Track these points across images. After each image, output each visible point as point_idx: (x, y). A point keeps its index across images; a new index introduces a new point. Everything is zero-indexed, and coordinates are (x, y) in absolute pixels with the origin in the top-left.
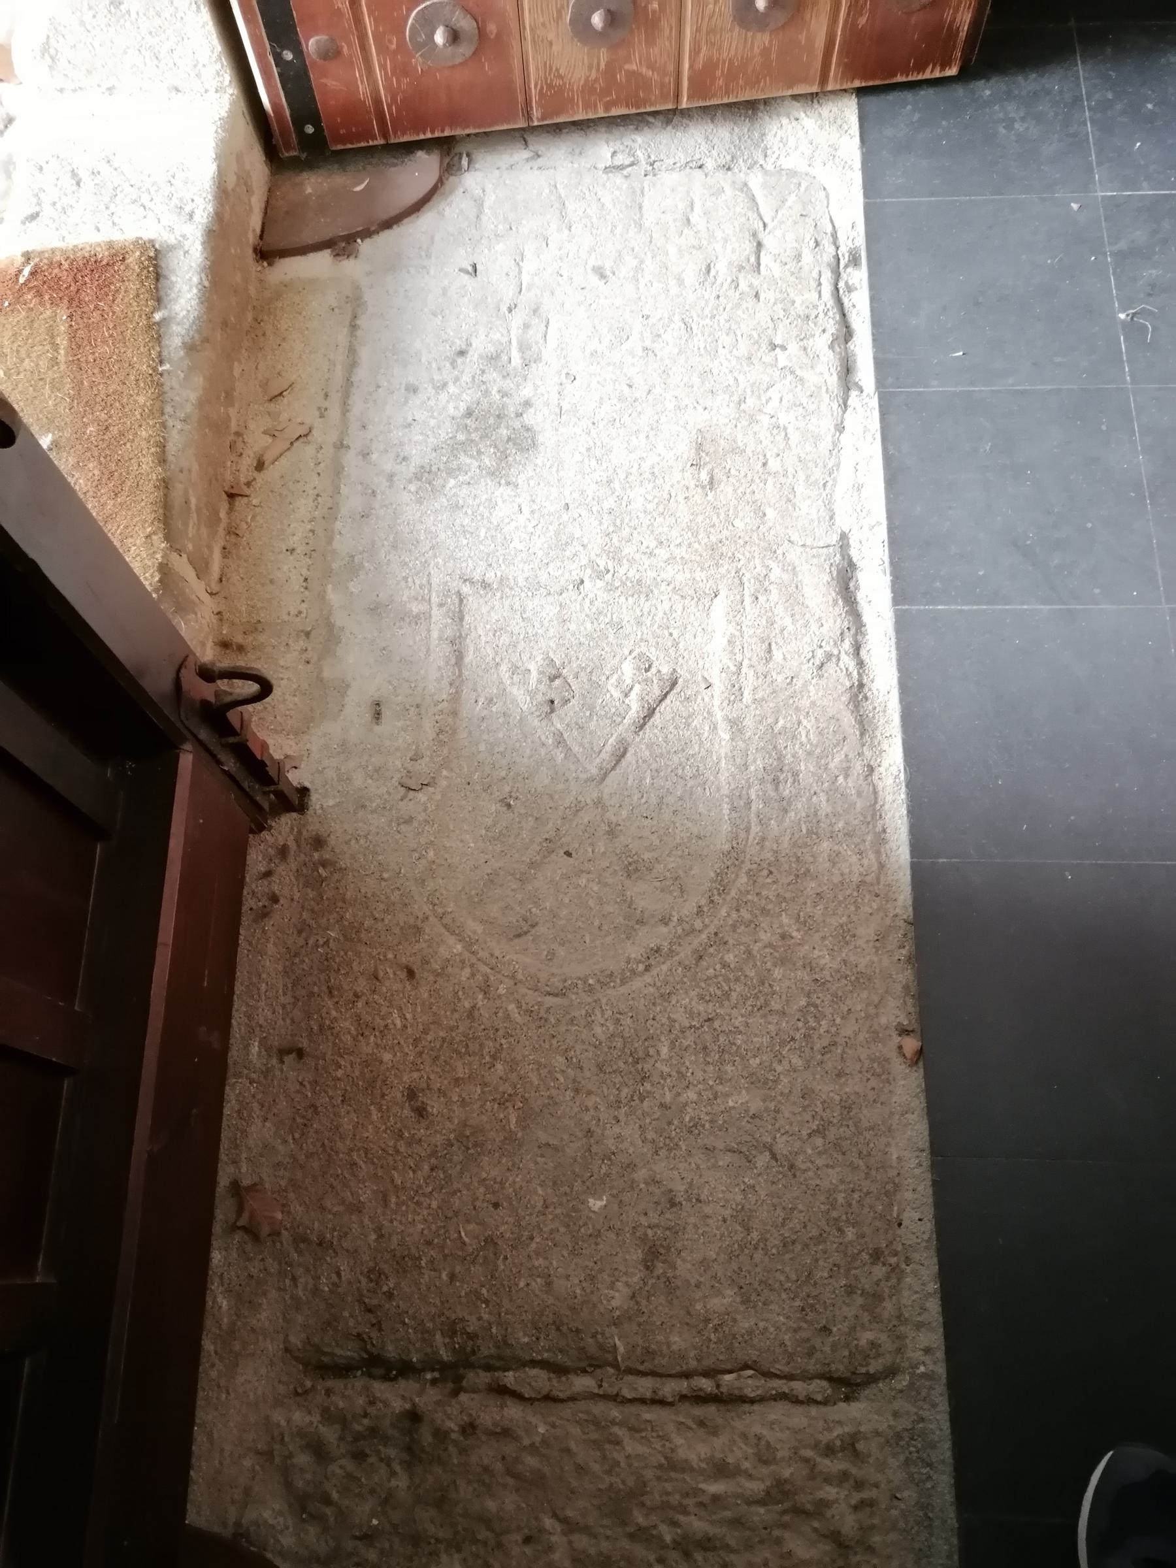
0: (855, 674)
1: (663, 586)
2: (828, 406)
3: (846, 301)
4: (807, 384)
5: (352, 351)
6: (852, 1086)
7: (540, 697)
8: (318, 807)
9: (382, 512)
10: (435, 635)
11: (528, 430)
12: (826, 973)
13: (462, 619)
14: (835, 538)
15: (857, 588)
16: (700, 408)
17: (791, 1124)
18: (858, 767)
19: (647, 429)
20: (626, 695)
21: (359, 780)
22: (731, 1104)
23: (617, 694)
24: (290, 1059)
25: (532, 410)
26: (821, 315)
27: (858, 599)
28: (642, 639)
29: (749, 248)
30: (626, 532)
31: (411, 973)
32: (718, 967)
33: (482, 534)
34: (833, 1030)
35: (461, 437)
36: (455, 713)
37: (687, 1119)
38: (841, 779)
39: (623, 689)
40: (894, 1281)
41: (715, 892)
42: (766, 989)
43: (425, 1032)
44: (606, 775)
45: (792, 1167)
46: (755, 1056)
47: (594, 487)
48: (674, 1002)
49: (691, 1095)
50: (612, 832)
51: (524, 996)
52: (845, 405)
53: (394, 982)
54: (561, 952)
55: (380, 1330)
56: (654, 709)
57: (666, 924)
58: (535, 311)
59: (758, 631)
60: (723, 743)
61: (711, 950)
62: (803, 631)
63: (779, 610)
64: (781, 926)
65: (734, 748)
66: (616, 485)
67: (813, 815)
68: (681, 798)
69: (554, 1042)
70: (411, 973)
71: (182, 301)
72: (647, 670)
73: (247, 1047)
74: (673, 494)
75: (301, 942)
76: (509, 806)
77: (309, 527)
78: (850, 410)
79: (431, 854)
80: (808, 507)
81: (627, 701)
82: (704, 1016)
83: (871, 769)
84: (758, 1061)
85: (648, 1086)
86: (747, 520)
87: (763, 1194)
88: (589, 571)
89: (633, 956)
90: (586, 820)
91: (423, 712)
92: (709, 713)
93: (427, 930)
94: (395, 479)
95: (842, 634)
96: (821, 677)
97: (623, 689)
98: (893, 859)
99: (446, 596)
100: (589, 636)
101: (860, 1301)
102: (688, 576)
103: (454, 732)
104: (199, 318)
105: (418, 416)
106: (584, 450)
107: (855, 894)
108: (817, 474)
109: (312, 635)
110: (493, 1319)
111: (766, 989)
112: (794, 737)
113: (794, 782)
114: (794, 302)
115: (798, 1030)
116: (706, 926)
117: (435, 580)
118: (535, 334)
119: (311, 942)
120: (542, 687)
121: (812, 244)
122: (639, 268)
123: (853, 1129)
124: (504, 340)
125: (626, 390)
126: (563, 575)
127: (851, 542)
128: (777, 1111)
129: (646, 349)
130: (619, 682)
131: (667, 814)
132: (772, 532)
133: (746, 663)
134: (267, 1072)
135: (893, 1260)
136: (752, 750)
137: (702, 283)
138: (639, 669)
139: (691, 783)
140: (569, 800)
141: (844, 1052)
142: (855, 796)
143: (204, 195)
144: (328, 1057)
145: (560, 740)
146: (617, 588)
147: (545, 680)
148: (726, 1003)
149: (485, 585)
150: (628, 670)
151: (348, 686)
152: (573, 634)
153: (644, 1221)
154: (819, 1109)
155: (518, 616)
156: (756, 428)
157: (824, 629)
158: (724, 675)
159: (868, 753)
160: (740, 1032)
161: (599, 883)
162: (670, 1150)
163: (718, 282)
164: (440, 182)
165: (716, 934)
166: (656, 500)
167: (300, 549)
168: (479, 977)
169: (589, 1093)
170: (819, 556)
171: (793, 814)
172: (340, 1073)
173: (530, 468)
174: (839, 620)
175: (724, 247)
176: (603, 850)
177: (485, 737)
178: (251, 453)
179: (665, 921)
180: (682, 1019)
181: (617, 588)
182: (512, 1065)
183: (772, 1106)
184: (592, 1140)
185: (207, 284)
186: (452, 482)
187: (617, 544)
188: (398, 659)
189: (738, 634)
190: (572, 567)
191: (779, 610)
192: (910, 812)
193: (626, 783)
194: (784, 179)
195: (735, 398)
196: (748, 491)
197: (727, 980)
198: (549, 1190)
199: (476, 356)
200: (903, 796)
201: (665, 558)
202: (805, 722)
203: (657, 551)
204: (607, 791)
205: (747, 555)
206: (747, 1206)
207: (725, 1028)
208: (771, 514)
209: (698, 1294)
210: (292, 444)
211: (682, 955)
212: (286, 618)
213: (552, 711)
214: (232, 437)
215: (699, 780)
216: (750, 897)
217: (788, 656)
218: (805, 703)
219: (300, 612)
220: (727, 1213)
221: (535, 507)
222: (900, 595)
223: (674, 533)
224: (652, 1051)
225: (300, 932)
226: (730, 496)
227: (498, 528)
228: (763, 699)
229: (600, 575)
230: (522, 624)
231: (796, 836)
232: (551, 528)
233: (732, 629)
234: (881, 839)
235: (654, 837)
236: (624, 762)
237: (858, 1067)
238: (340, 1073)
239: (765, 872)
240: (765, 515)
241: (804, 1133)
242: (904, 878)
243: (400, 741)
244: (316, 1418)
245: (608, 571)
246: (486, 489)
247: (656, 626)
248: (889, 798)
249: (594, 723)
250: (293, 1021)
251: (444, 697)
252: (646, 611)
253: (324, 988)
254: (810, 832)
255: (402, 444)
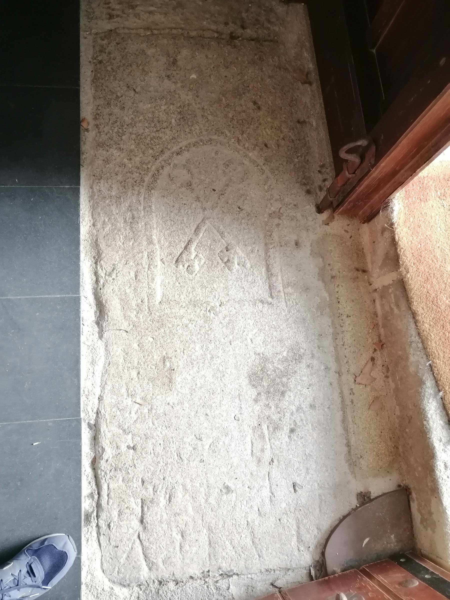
0: (98, 268)
1: (184, 305)
2: (106, 412)
3: (94, 487)
4: (117, 424)
5: (346, 429)
6: (106, 111)
7: (233, 251)
8: (312, 206)
9: (313, 337)
10: (280, 278)
11: (253, 385)
12: (114, 147)
13: (270, 286)
14: (105, 335)
15: (96, 312)
16: (171, 404)
17: (128, 100)
18: (99, 225)
19: (197, 389)
20: (197, 255)
21: (299, 216)
22: (149, 105)
23: (200, 255)
24: (302, 120)
25: (254, 397)
26: (108, 472)
27: (95, 307)
28: (192, 280)
29: (148, 519)
30: (203, 330)
31: (266, 145)
32: (155, 148)
33: (267, 327)
34: (113, 128)
35: (284, 380)
36: (266, 244)
37: (164, 101)
38: (106, 220)
39: (198, 258)
40: (95, 56)
41: (157, 174)
42: (137, 141)
43: (257, 127)
44: (203, 220)
45: (128, 87)
46: (141, 120)
47: (220, 355)
48: (171, 137)
49: (163, 108)
50: (198, 199)
51: (225, 138)
52: (98, 413)
53: (272, 144)
54: (213, 154)
55: (257, 47)
56: (184, 249)
57: (174, 164)
58: (259, 461)
59: (141, 285)
60: (155, 235)
61: (157, 154)
62: (121, 286)
63: (132, 296)
64: (131, 163)
65: (150, 232)
66: (209, 356)
67: (118, 204)
68: (172, 212)
69: (212, 124)
70: (266, 145)
71: (433, 408)
72: (189, 266)
73: (317, 124)
74: (182, 353)
75: (307, 158)
76: (239, 208)
77: (343, 329)
78: (95, 410)
79: (266, 188)
80: (117, 351)
81: (196, 252)
82: (160, 132)
83: (94, 225)
84: (140, 118)
85: (179, 110)
86: (147, 341)
87: (138, 79)
88: (218, 310)
89: (186, 152)
90: (208, 203)
91: (279, 244)
92: (161, 248)
93: (263, 160)
94: (311, 355)
95: (104, 286)
96: (114, 265)
97: (198, 258)
98: (87, 190)
99: (278, 296)
100: (214, 281)
101: (107, 51)
102: (173, 311)
103: (265, 237)
104: (422, 400)
105: (306, 390)
106: (226, 374)
107: (102, 175)
108: (112, 370)
109: (330, 277)
110: (223, 48)
111: (137, 141)
112: (126, 237)
113: (126, 219)
114: (123, 480)
115: (126, 128)
116: (160, 162)
117: (284, 304)
118: (258, 446)
119: (303, 158)
120: (232, 256)
121: (112, 525)
122: (208, 495)
123: (107, 98)
124: (272, 441)
125: (208, 412)
126: (229, 309)
127: (97, 335)
128: (133, 103)
129: (200, 439)
130: (200, 260)
131: (177, 205)
132: (135, 336)
133: (146, 270)
134: (308, 117)
135: (95, 61)
136: (143, 231)
137: (173, 488)
138: (192, 266)
139: (168, 218)
140: (216, 211)
141: (109, 122)
142: (101, 213)
143: (443, 481)
144: (289, 121)
145: (222, 234)
146: (204, 303)
147: (231, 259)
148: (152, 137)
149: (262, 302)
150: (197, 267)
151: (311, 254)
152: (221, 282)
153: (178, 72)
154: (118, 104)
155: (246, 289)
156: (143, 394)
157: (112, 287)
158: (156, 264)
159: (95, 231)
160: (146, 127)
161: (201, 180)
162: (170, 91)
163: (164, 490)
164: (323, 554)
165: (156, 159)
166: (190, 349)
167: (344, 317)
168: (242, 144)
169: (199, 109)
170: (113, 325)
171: (126, 205)
172: (284, 116)
173: (250, 364)
174: (105, 293)
175: (162, 516)
176: (201, 192)
177: (252, 236)
178: (379, 367)
179: (175, 166)
180: (168, 131)
181: (204, 303)
182: (226, 116)
183: (135, 105)
184: (196, 94)
185: (425, 423)
186: (285, 354)
187: (206, 324)
188: (293, 267)
189: (150, 283)
190: (225, 312)
191: (132, 296)
192: (79, 205)
193: (194, 218)
194: (128, 576)
195: (154, 411)
196: (146, 357)
197: (152, 144)
198: (209, 80)
199: (285, 429)
200: (81, 212)
201: (184, 319)
202: (121, 244)
203: (188, 322)
204: (201, 215)
205: (146, 323)
206: (143, 76)
207: (152, 129)
208: (135, 346)
209: (159, 53)
210: (362, 372)
211: (169, 153)
212: (342, 284)
213: (227, 247)
214: (389, 374)
215: (164, 219)
216: (143, 173)
217: (128, 274)
218: (121, 252)
219: (338, 287)
220: (150, 74)
221: (245, 342)
222: (77, 301)
223: (180, 331)
224: (178, 121)
225: (308, 161)
226: (155, 354)
227: (260, 330)
228: (139, 253)
229: (212, 308)
230: (244, 286)
231: (125, 196)
232: (237, 331)
233: (153, 286)
234: (91, 197)
235: (181, 196)
236: (195, 226)
237: (104, 117)
238: (284, 116)
239: (137, 182)
240: (138, 345)
241: (124, 97)
242: (82, 181)
243: (286, 232)
244: (272, 28)
245: (209, 311)
246: (269, 351)
247: (186, 287)
248: (87, 213)
249: (209, 243)
250: (304, 131)
251: (271, 250)
252: (191, 294)
253: (295, 142)
254: (120, 198)
255: (311, 375)
